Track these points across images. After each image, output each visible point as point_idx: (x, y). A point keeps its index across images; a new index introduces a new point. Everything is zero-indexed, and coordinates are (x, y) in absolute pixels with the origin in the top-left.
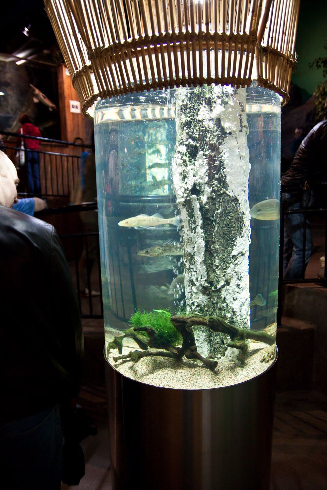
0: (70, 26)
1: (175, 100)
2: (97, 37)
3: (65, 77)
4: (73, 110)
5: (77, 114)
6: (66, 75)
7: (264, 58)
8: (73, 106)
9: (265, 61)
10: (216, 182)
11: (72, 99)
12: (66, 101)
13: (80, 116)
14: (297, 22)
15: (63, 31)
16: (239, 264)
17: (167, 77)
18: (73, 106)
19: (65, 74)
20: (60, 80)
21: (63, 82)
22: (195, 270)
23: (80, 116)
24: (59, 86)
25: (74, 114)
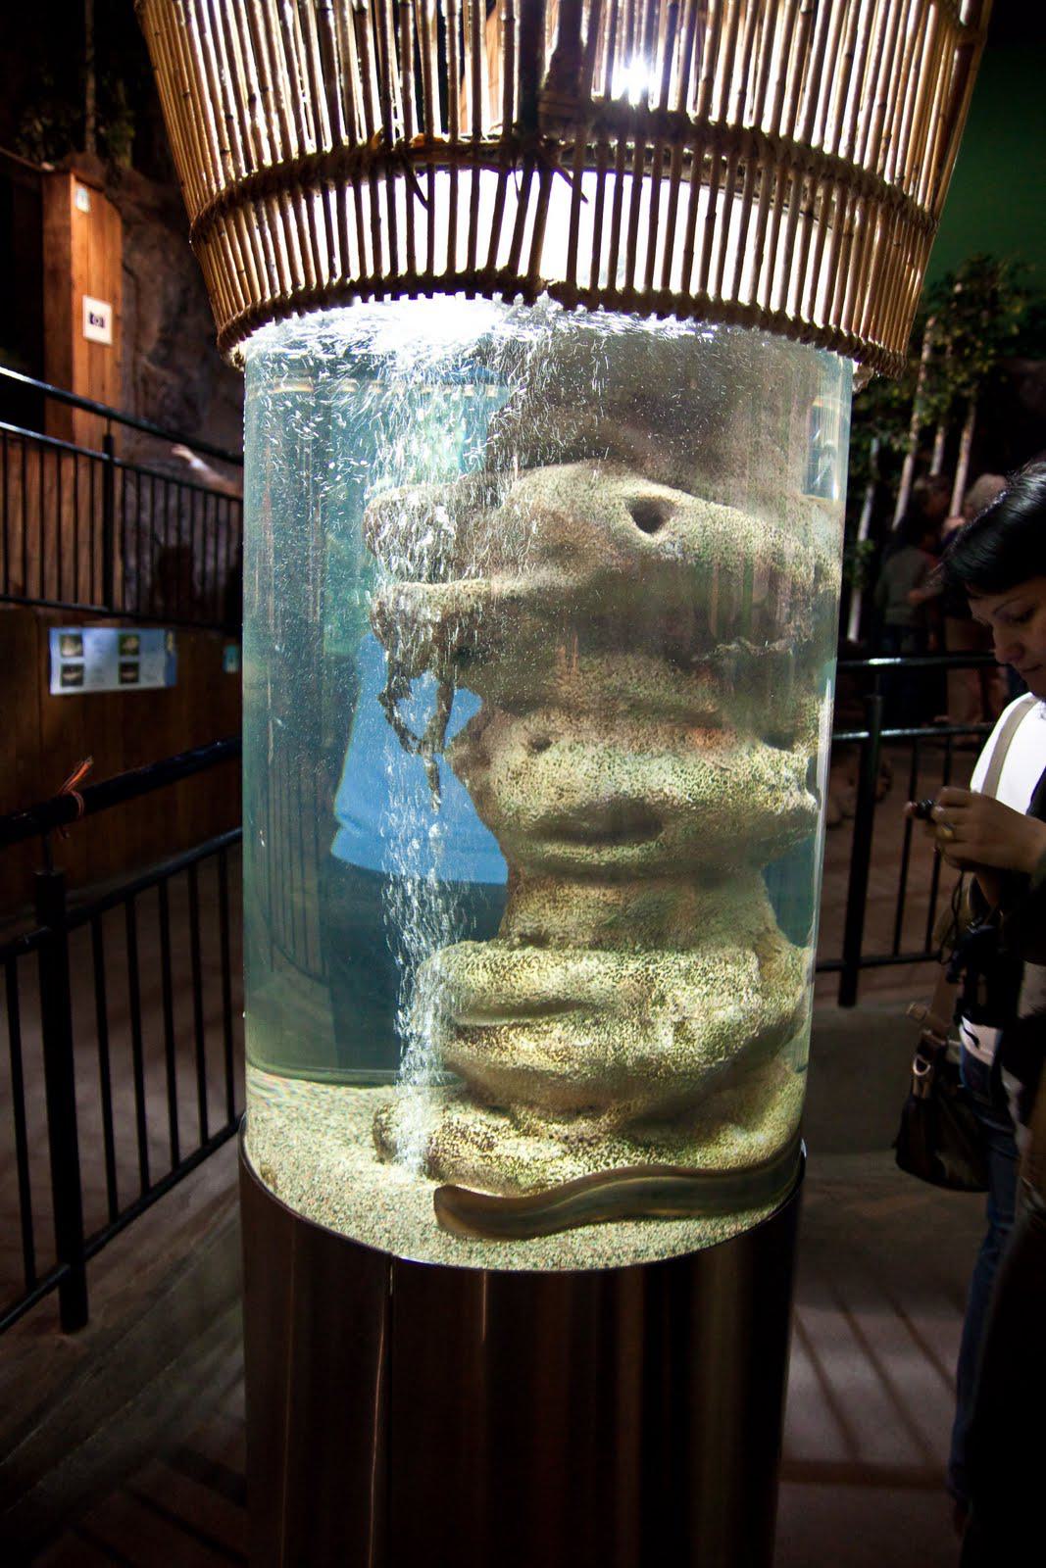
0: (649, 203)
1: (550, 370)
2: (224, 90)
3: (74, 215)
4: (92, 332)
5: (102, 346)
6: (79, 211)
7: (80, 199)
8: (92, 316)
9: (819, 218)
10: (780, 811)
11: (89, 294)
12: (75, 296)
13: (108, 352)
14: (937, 158)
15: (203, 93)
16: (913, 1331)
17: (724, 191)
18: (92, 316)
19: (77, 208)
20: (52, 221)
21: (67, 230)
22: (575, 1252)
23: (108, 352)
24: (48, 239)
25: (91, 343)
